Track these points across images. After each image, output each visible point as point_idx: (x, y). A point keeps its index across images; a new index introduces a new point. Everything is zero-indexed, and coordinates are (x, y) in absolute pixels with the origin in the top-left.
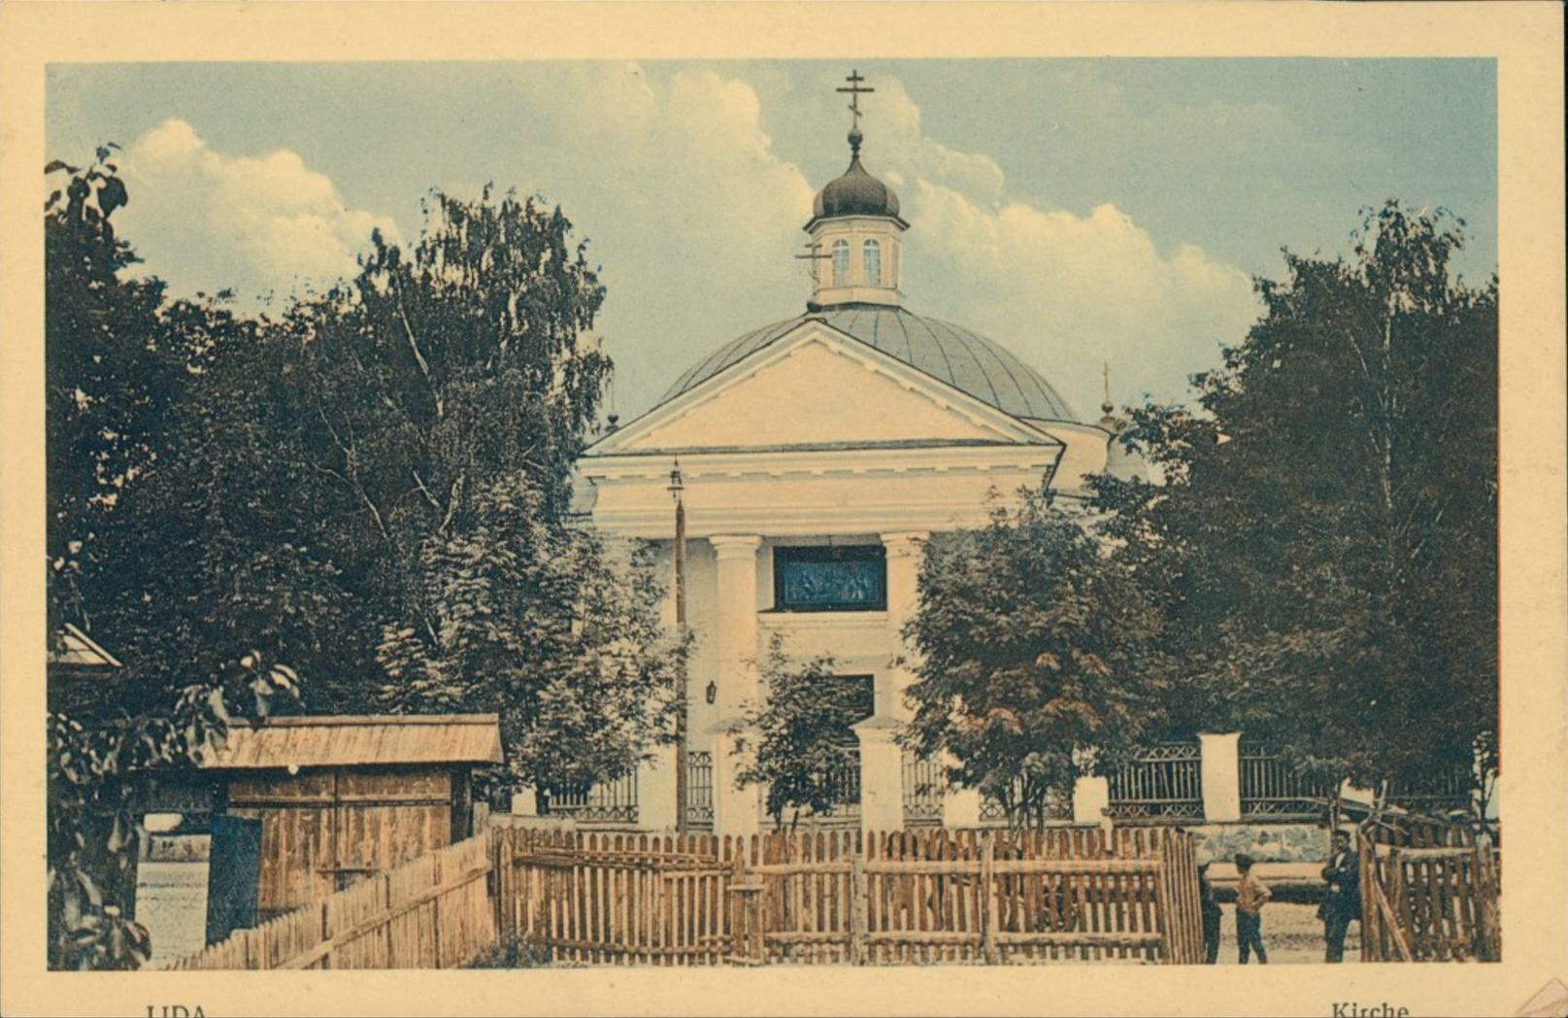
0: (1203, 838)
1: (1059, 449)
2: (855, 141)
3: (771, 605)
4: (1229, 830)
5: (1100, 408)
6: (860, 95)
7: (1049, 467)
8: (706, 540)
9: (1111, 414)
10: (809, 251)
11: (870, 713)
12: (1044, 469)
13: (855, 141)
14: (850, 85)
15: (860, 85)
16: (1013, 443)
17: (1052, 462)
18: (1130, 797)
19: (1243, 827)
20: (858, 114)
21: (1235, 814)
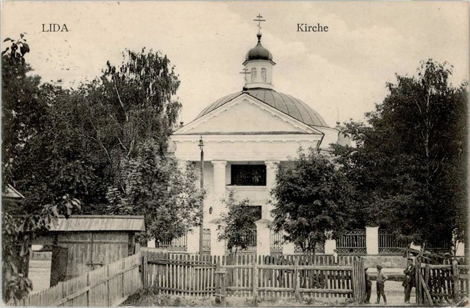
0: (366, 260)
1: (322, 135)
2: (259, 37)
3: (230, 183)
4: (375, 258)
5: (336, 123)
6: (261, 22)
7: (319, 141)
8: (210, 162)
9: (340, 125)
10: (244, 71)
11: (260, 218)
12: (317, 142)
13: (259, 37)
14: (258, 19)
15: (261, 19)
16: (308, 134)
17: (320, 139)
18: (343, 246)
19: (380, 256)
20: (260, 28)
21: (377, 252)
